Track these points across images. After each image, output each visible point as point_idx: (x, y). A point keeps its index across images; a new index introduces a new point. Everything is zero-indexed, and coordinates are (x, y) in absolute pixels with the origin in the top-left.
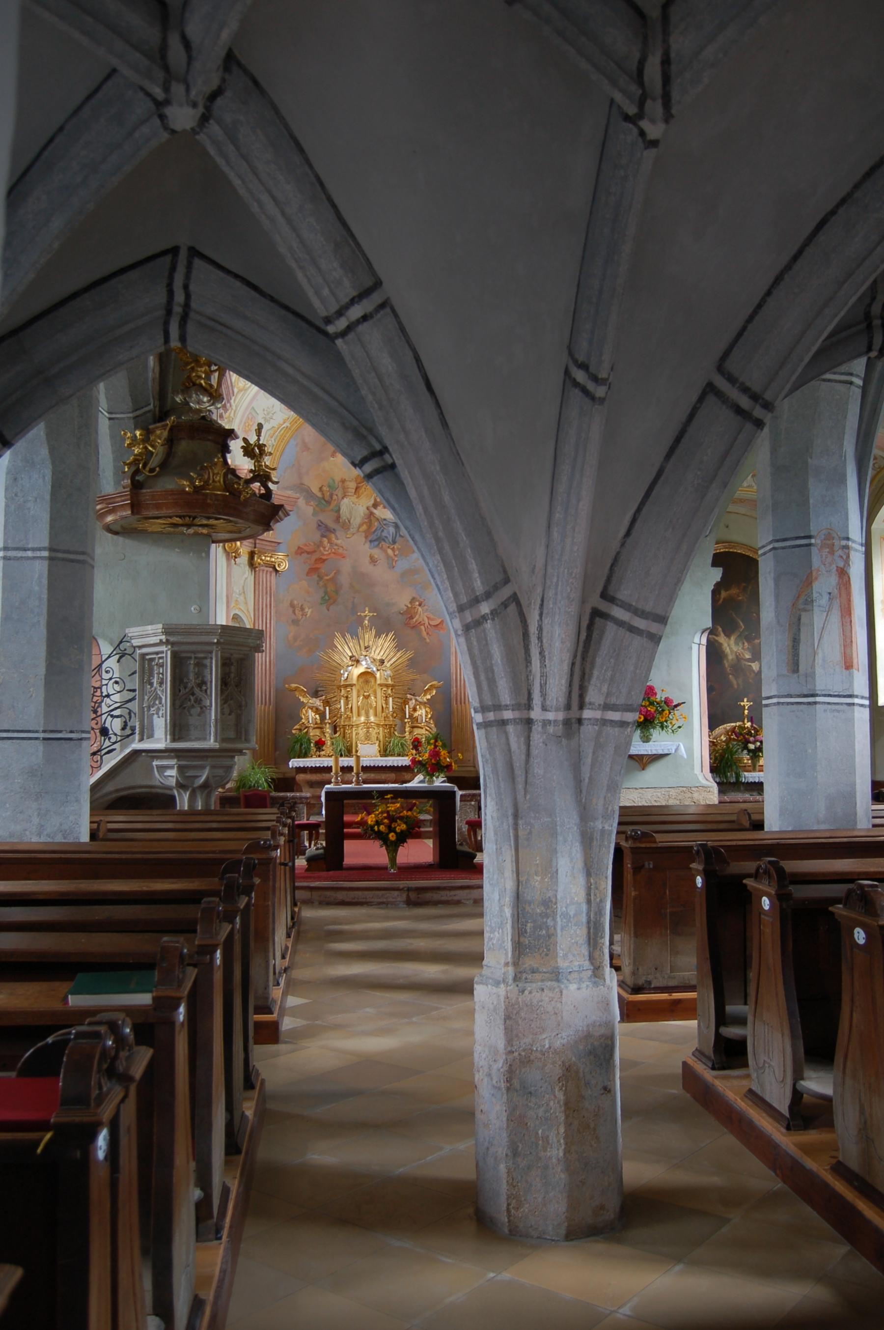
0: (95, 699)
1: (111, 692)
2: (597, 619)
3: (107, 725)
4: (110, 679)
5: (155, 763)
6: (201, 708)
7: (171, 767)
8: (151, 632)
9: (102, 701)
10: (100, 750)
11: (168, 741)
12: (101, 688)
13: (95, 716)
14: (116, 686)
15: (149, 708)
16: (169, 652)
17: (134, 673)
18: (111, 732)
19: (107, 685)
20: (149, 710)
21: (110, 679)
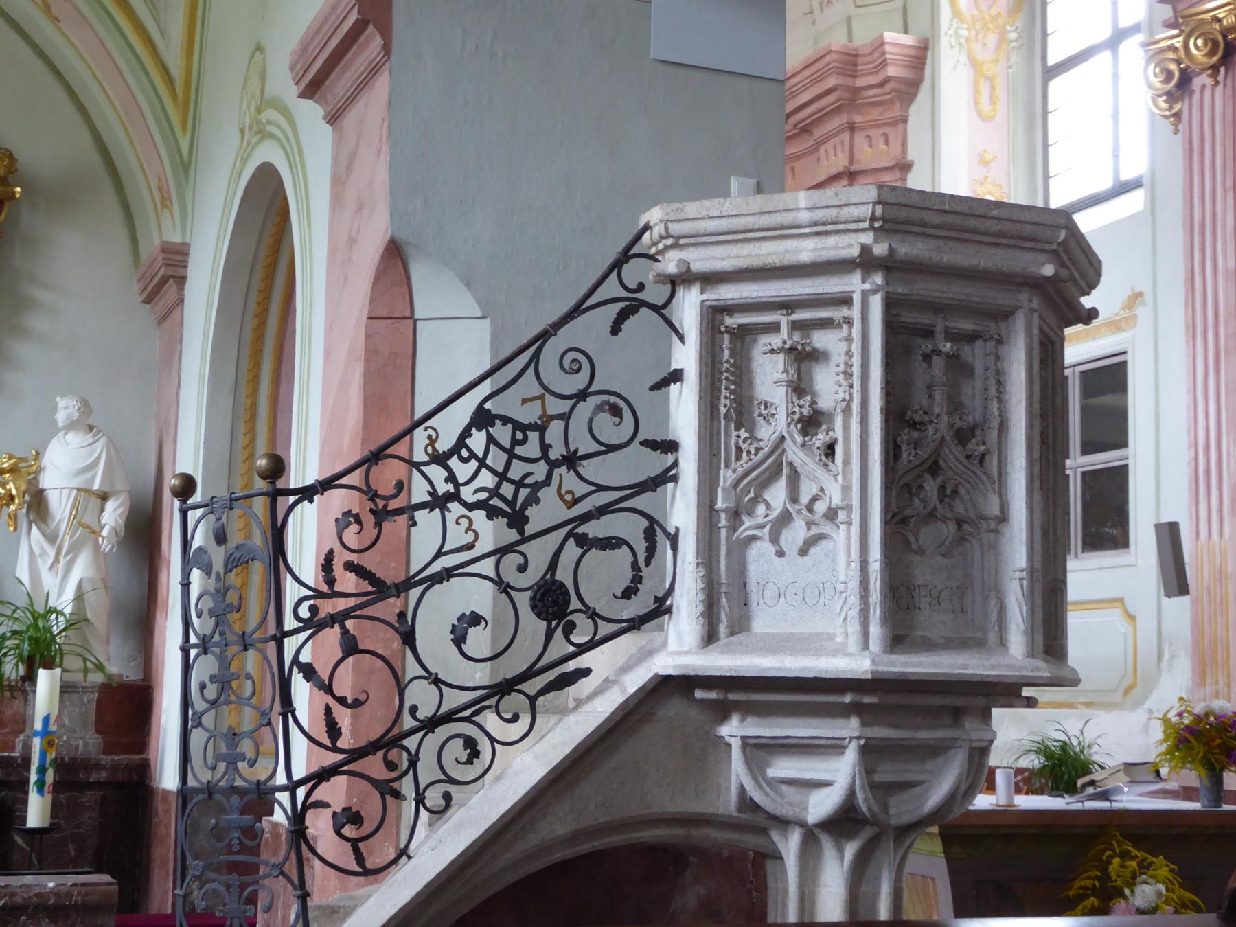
0: (516, 472)
1: (584, 445)
2: (279, 498)
3: (564, 575)
4: (582, 395)
5: (733, 730)
6: (959, 523)
7: (835, 748)
8: (804, 217)
9: (547, 482)
10: (529, 674)
11: (875, 644)
12: (541, 429)
13: (513, 536)
14: (605, 421)
15: (735, 515)
17: (676, 376)
18: (575, 604)
19: (566, 417)
20: (733, 529)
21: (582, 395)
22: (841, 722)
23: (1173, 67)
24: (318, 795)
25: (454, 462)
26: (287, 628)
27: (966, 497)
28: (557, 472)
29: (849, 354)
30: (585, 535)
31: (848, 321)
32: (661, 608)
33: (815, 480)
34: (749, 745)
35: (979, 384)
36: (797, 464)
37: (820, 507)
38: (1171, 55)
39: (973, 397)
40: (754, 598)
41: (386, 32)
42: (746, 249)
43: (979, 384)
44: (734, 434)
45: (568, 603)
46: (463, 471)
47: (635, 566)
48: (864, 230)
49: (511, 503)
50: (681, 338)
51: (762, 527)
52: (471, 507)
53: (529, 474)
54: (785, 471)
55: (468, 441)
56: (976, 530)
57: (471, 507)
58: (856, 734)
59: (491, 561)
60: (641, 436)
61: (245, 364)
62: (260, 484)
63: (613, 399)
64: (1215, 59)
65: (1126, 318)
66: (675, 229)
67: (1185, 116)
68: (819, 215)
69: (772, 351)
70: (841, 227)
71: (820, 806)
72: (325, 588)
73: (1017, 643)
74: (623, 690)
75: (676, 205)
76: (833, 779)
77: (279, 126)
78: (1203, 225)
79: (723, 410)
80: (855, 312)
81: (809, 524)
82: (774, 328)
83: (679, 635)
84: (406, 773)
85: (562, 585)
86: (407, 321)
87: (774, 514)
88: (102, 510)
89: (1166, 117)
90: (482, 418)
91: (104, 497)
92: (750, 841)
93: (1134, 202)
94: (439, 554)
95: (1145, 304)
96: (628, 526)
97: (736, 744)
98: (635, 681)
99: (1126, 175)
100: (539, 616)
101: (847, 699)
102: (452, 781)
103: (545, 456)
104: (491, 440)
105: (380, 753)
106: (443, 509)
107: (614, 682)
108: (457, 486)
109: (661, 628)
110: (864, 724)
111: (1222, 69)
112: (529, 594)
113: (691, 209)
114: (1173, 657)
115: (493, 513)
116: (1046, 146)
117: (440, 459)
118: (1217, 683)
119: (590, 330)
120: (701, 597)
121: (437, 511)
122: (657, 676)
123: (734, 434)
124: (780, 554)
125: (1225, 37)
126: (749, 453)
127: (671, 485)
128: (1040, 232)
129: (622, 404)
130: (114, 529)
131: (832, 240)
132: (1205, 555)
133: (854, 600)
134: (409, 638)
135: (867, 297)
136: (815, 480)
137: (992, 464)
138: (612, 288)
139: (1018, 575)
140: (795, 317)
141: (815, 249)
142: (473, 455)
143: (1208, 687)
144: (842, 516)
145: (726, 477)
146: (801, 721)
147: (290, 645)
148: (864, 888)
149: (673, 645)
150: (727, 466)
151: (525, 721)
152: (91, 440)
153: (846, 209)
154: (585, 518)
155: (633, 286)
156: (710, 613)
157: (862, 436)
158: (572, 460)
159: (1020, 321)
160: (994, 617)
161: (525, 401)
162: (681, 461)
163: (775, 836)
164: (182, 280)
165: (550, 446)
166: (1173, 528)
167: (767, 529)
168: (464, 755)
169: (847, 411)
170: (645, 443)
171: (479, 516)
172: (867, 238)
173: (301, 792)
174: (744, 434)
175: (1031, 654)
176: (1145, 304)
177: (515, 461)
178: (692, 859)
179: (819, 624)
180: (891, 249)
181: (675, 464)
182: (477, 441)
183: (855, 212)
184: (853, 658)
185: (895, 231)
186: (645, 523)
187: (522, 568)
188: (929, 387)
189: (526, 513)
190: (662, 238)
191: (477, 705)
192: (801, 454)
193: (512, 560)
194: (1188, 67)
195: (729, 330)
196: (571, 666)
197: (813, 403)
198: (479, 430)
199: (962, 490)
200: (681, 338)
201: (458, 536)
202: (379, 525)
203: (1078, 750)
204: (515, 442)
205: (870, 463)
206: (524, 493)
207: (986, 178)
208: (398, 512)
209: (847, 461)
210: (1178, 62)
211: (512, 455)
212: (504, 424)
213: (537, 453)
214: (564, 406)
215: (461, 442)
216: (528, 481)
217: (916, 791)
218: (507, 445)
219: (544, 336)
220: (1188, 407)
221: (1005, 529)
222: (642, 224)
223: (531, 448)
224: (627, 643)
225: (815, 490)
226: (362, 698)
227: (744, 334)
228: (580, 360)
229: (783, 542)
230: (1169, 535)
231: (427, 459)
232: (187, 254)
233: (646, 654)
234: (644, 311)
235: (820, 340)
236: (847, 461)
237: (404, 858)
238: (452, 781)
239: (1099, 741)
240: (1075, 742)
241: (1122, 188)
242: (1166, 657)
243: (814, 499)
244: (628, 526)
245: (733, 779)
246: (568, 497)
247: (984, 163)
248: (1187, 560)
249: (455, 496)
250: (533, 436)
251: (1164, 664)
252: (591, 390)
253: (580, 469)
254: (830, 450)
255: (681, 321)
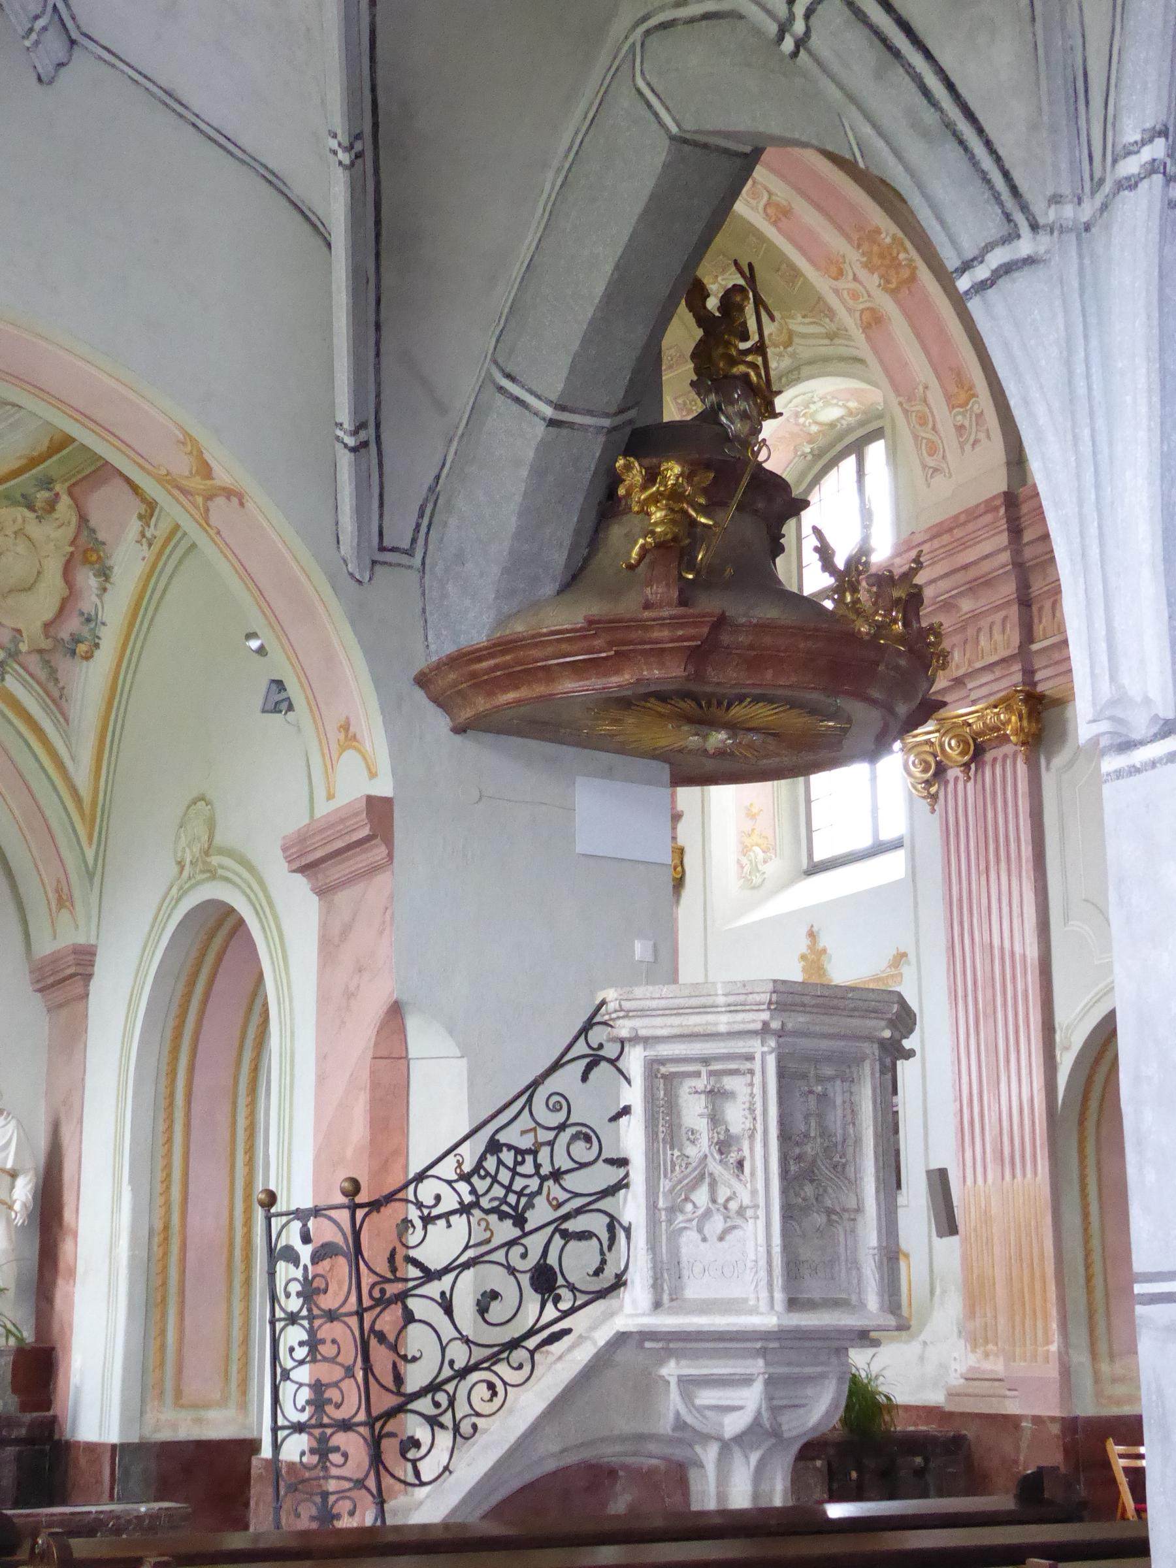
0: (518, 1184)
1: (563, 1163)
3: (552, 1260)
4: (562, 1127)
5: (671, 1370)
7: (747, 1381)
9: (539, 1192)
11: (779, 1305)
12: (534, 1152)
13: (517, 1232)
15: (673, 1210)
16: (771, 1061)
17: (626, 1111)
18: (560, 1281)
19: (551, 1144)
20: (670, 1222)
21: (562, 1127)
22: (749, 1362)
23: (930, 759)
24: (389, 1428)
25: (475, 1180)
26: (365, 1306)
27: (833, 1195)
28: (546, 1184)
29: (752, 1095)
30: (566, 1230)
31: (751, 1072)
32: (619, 1282)
33: (730, 1186)
34: (683, 1381)
35: (839, 1112)
36: (716, 1174)
37: (733, 1206)
38: (927, 748)
39: (835, 1122)
40: (685, 1273)
41: (389, 842)
42: (676, 1021)
43: (839, 1112)
44: (669, 1153)
45: (556, 1280)
46: (481, 1185)
47: (602, 1253)
48: (763, 1010)
49: (515, 1208)
50: (629, 1082)
51: (691, 1220)
52: (487, 1212)
53: (526, 1187)
54: (707, 1180)
55: (484, 1164)
56: (841, 1217)
57: (487, 1212)
58: (762, 1370)
59: (503, 1251)
60: (603, 1157)
61: (165, 1059)
62: (344, 1200)
63: (584, 1130)
64: (966, 758)
65: (892, 976)
66: (627, 1005)
67: (941, 795)
68: (731, 999)
69: (696, 1092)
70: (748, 1007)
71: (733, 1425)
72: (389, 1276)
73: (873, 1302)
74: (595, 1343)
75: (626, 989)
76: (748, 1402)
77: (227, 869)
78: (960, 900)
79: (661, 1136)
80: (757, 1065)
81: (726, 1218)
82: (698, 1074)
83: (634, 1302)
84: (445, 1411)
85: (551, 1268)
86: (403, 1061)
87: (700, 1212)
88: (13, 1187)
89: (924, 797)
90: (494, 1147)
91: (13, 1175)
92: (678, 1453)
93: (893, 866)
94: (467, 1247)
95: (909, 964)
96: (595, 1223)
97: (673, 1382)
98: (602, 1336)
99: (886, 835)
100: (536, 1291)
101: (759, 1345)
102: (478, 1415)
103: (537, 1173)
104: (500, 1162)
105: (430, 1396)
106: (469, 1213)
107: (586, 1338)
108: (478, 1197)
109: (618, 1297)
110: (767, 1364)
111: (973, 766)
112: (528, 1275)
113: (639, 991)
114: (944, 1292)
115: (503, 1216)
116: (808, 801)
117: (465, 1178)
118: (985, 1316)
119: (567, 1080)
120: (651, 1273)
121: (464, 1216)
122: (618, 1332)
123: (669, 1153)
124: (704, 1240)
125: (974, 740)
126: (681, 1166)
127: (623, 1191)
128: (880, 1006)
129: (592, 1134)
130: (24, 1205)
131: (740, 1017)
132: (972, 1200)
133: (763, 1274)
134: (448, 1309)
135: (765, 1058)
136: (730, 1186)
137: (850, 1171)
138: (580, 1048)
139: (871, 1252)
140: (711, 1068)
141: (728, 1023)
142: (488, 1174)
143: (978, 1320)
144: (749, 1213)
145: (665, 1185)
146: (721, 1362)
147: (368, 1317)
148: (763, 1487)
149: (628, 1308)
150: (665, 1176)
151: (527, 1368)
152: (3, 1123)
153: (751, 996)
154: (566, 1217)
155: (595, 1046)
156: (656, 1285)
157: (764, 1158)
158: (557, 1175)
159: (867, 1068)
160: (855, 1281)
161: (523, 1133)
162: (631, 1173)
163: (698, 1449)
164: (89, 976)
165: (540, 1165)
166: (942, 1174)
167: (695, 1223)
168: (487, 1394)
169: (752, 1137)
170: (607, 1161)
171: (493, 1218)
172: (765, 1016)
173: (378, 1425)
174: (676, 1153)
175: (882, 1308)
176: (909, 964)
177: (517, 1178)
178: (621, 1473)
179: (735, 1291)
180: (783, 1024)
181: (627, 1175)
182: (490, 1164)
183: (757, 998)
184: (767, 1316)
185: (784, 1011)
186: (607, 1220)
187: (524, 1256)
188: (807, 1117)
189: (526, 1215)
190: (616, 1011)
191: (494, 1359)
192: (719, 1168)
193: (517, 1251)
194: (941, 761)
195: (664, 1076)
196: (556, 1328)
197: (727, 1130)
198: (492, 1155)
199: (830, 1190)
200: (629, 1082)
201: (479, 1235)
202: (425, 1228)
203: (866, 1381)
204: (516, 1163)
205: (771, 1176)
206: (523, 1200)
207: (753, 830)
208: (439, 1217)
209: (753, 1174)
210: (935, 756)
211: (515, 1173)
212: (509, 1150)
213: (532, 1171)
214: (550, 1135)
215: (479, 1165)
216: (527, 1191)
217: (801, 1411)
218: (511, 1166)
219: (535, 1084)
220: (953, 1063)
221: (859, 1219)
222: (597, 1002)
223: (528, 1168)
224: (599, 1306)
225: (729, 1193)
226: (418, 1355)
227: (669, 1078)
228: (561, 1102)
229: (706, 1231)
230: (939, 1180)
231: (455, 1177)
232: (94, 954)
233: (612, 1314)
234: (603, 1064)
235: (730, 1083)
236: (753, 1174)
237: (447, 1473)
238: (478, 1415)
239: (884, 1373)
240: (863, 1375)
241: (879, 849)
242: (938, 1291)
243: (728, 1200)
244: (595, 1223)
245: (671, 1408)
246: (554, 1203)
247: (752, 816)
248: (955, 1204)
249: (476, 1204)
250: (529, 1159)
251: (936, 1299)
252: (527, 1108)
253: (562, 1182)
254: (740, 1164)
255: (628, 1070)
